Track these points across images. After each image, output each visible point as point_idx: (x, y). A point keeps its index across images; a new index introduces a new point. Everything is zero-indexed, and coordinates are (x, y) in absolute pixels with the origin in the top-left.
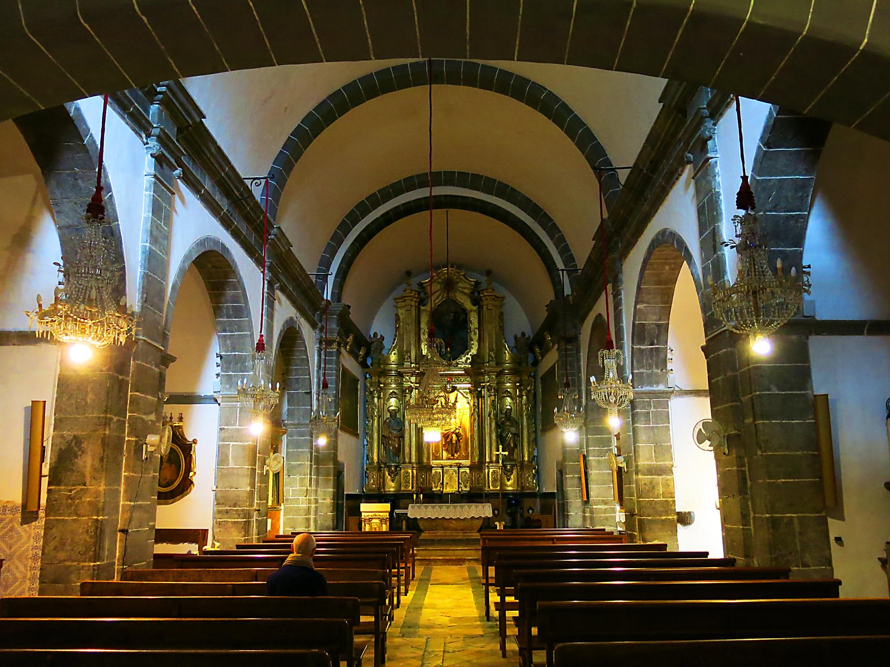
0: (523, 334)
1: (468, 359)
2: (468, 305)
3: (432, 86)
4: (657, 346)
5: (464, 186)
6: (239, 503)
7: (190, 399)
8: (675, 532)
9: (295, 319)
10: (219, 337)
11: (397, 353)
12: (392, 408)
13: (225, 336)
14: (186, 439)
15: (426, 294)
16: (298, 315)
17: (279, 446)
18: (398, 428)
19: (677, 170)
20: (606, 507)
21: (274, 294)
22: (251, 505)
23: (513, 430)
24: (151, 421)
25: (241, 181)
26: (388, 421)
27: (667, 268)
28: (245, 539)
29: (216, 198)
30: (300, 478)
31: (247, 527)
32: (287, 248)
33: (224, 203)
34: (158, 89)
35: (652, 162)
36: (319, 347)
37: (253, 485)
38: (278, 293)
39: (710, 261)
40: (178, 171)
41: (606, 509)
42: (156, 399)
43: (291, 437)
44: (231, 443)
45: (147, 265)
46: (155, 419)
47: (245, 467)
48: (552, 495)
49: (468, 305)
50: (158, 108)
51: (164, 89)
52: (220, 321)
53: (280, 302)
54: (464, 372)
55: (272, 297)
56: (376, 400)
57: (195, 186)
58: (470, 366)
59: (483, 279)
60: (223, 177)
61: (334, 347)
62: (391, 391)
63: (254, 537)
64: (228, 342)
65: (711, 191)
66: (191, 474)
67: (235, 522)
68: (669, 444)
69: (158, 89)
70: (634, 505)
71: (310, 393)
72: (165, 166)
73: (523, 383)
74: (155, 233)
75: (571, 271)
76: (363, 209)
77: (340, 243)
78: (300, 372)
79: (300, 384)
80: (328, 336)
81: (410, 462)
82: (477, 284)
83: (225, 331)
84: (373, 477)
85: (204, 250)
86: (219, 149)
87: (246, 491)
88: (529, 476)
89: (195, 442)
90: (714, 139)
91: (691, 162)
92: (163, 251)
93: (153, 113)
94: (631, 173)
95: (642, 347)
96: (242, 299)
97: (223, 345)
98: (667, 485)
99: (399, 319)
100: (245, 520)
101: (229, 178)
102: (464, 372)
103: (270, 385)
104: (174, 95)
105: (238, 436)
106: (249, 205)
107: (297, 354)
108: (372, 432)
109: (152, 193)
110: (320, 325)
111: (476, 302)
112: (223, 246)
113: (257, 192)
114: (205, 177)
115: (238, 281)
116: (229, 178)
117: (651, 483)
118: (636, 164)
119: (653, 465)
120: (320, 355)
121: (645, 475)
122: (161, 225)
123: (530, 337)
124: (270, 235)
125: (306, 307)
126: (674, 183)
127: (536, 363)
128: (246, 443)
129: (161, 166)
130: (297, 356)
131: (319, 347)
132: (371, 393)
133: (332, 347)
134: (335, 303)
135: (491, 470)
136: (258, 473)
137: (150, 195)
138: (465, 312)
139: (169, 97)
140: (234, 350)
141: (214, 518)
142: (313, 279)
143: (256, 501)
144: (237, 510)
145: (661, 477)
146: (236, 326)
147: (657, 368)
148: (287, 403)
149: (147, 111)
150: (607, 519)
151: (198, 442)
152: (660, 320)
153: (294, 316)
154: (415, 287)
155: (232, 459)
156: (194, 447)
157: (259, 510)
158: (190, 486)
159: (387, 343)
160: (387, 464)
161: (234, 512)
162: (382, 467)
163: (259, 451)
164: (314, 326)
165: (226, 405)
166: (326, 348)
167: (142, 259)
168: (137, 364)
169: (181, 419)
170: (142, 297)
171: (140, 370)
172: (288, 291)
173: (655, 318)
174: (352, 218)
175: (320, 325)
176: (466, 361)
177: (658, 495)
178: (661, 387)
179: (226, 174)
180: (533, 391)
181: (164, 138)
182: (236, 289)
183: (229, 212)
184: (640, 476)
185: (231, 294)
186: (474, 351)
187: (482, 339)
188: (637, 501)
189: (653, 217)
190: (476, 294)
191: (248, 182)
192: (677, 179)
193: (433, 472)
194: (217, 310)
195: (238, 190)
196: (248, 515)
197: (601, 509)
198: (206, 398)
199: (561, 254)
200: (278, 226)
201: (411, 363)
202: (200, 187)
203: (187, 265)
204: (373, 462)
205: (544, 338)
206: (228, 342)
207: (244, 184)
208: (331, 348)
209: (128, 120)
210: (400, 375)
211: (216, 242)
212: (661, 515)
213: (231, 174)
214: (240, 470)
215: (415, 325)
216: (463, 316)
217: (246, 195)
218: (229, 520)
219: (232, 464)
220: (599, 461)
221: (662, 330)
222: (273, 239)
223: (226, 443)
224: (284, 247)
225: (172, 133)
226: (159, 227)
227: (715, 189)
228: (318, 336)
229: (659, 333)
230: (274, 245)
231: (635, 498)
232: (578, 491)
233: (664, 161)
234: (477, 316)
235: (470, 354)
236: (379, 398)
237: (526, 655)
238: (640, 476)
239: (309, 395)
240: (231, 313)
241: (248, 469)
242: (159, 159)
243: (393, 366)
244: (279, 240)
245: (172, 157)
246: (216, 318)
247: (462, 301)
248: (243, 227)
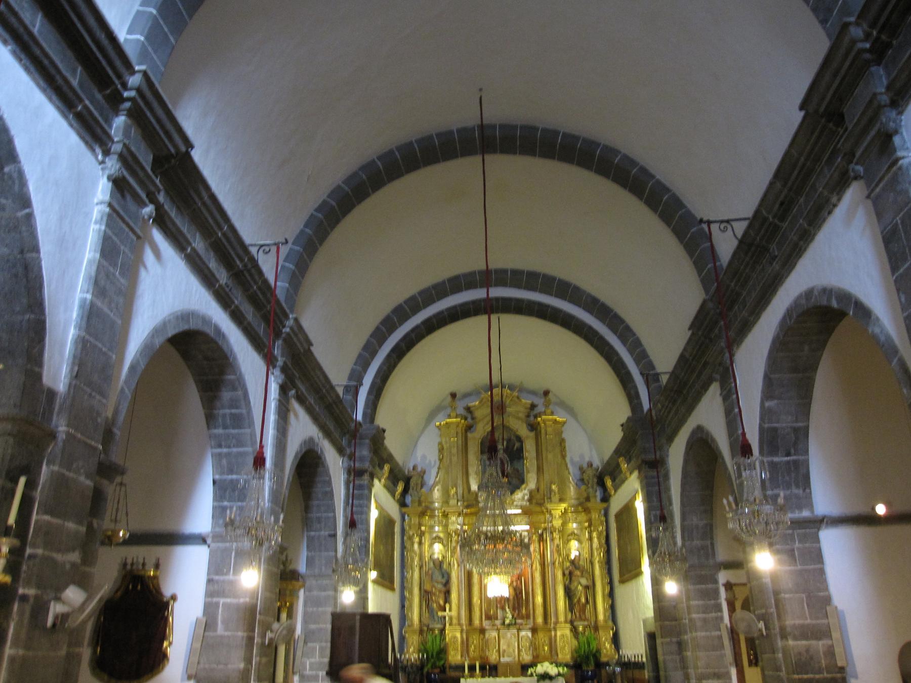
0: (590, 465)
1: (524, 495)
2: (523, 431)
3: (486, 157)
7: (174, 539)
16: (321, 435)
19: (828, 201)
23: (584, 581)
25: (244, 247)
32: (307, 347)
33: (223, 276)
34: (126, 94)
35: (782, 204)
37: (248, 660)
38: (295, 405)
40: (149, 209)
48: (639, 666)
49: (523, 431)
50: (125, 122)
51: (133, 94)
53: (296, 415)
57: (178, 241)
59: (540, 401)
60: (220, 239)
66: (165, 644)
69: (126, 94)
72: (128, 197)
74: (102, 283)
76: (401, 313)
77: (373, 354)
78: (323, 509)
79: (323, 524)
83: (220, 446)
86: (213, 198)
89: (174, 598)
90: (902, 134)
91: (862, 178)
93: (116, 128)
94: (750, 227)
96: (243, 403)
98: (830, 652)
103: (272, 518)
104: (147, 103)
105: (229, 589)
106: (256, 283)
110: (348, 451)
111: (533, 427)
112: (218, 330)
113: (268, 266)
120: (347, 488)
125: (332, 428)
126: (824, 220)
129: (123, 196)
138: (519, 439)
140: (231, 472)
142: (340, 391)
148: (306, 549)
149: (109, 122)
152: (797, 421)
159: (431, 478)
164: (341, 451)
167: (78, 315)
169: (157, 566)
170: (72, 370)
171: (60, 483)
174: (388, 325)
175: (348, 451)
176: (523, 498)
178: (806, 514)
181: (130, 159)
182: (234, 389)
184: (791, 642)
189: (786, 277)
190: (532, 418)
191: (253, 250)
192: (830, 213)
194: (210, 418)
195: (242, 260)
199: (637, 361)
202: (185, 244)
203: (159, 341)
206: (224, 461)
209: (73, 122)
210: (446, 515)
211: (206, 320)
213: (230, 235)
215: (462, 458)
216: (517, 445)
219: (220, 630)
221: (801, 436)
225: (146, 159)
226: (111, 277)
228: (346, 464)
229: (797, 438)
230: (289, 343)
233: (802, 200)
242: (118, 184)
244: (296, 335)
245: (142, 189)
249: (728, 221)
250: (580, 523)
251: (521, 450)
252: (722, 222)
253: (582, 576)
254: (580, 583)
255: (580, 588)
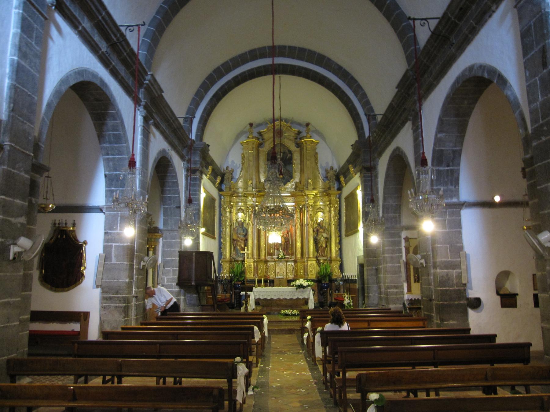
0: (332, 168)
2: (292, 147)
4: (452, 168)
5: (293, 57)
9: (167, 151)
10: (104, 160)
11: (242, 181)
12: (240, 220)
13: (108, 159)
14: (77, 241)
15: (263, 139)
16: (170, 148)
18: (243, 234)
19: (490, 7)
20: (397, 290)
21: (149, 128)
22: (130, 293)
23: (325, 235)
24: (20, 223)
26: (236, 229)
27: (466, 102)
28: (125, 320)
29: (95, 39)
31: (126, 310)
33: (104, 46)
36: (186, 174)
37: (131, 277)
38: (153, 129)
39: (537, 78)
41: (397, 292)
42: (26, 204)
43: (166, 239)
44: (114, 244)
45: (14, 77)
46: (25, 222)
49: (292, 147)
52: (104, 146)
54: (290, 195)
57: (73, 23)
58: (294, 190)
60: (100, 20)
61: (198, 174)
62: (239, 208)
63: (133, 317)
64: (111, 164)
65: (541, 11)
66: (82, 268)
67: (116, 307)
68: (461, 245)
71: (179, 207)
73: (332, 202)
74: (24, 49)
77: (202, 98)
79: (172, 201)
81: (253, 258)
83: (108, 154)
84: (226, 268)
85: (82, 79)
87: (126, 282)
88: (336, 267)
89: (85, 243)
92: (34, 68)
94: (439, 23)
95: (441, 168)
96: (120, 128)
97: (107, 167)
99: (244, 157)
100: (124, 305)
101: (106, 22)
102: (290, 195)
105: (119, 238)
106: (126, 51)
107: (170, 178)
108: (225, 236)
109: (21, 11)
111: (299, 145)
112: (102, 81)
114: (84, 18)
115: (116, 113)
116: (106, 22)
118: (445, 14)
119: (449, 261)
122: (31, 44)
123: (336, 169)
124: (145, 80)
127: (340, 189)
131: (186, 174)
132: (225, 209)
133: (196, 174)
134: (198, 142)
136: (136, 267)
137: (19, 13)
140: (115, 170)
141: (101, 303)
142: (181, 121)
144: (118, 297)
145: (455, 271)
146: (116, 151)
147: (452, 185)
150: (398, 299)
152: (455, 146)
153: (167, 149)
155: (114, 256)
156: (85, 247)
157: (136, 297)
158: (82, 277)
160: (236, 259)
161: (116, 299)
162: (232, 261)
163: (136, 250)
164: (182, 158)
165: (110, 214)
166: (190, 175)
167: (10, 71)
168: (3, 169)
169: (74, 225)
170: (9, 107)
172: (161, 128)
173: (451, 144)
176: (292, 187)
178: (455, 200)
179: (103, 18)
180: (338, 208)
182: (115, 119)
183: (107, 53)
185: (111, 124)
186: (297, 180)
190: (299, 140)
192: (490, 16)
193: (268, 264)
194: (101, 137)
195: (115, 36)
197: (394, 292)
198: (95, 208)
199: (363, 107)
200: (151, 73)
201: (253, 188)
202: (77, 24)
203: (64, 88)
206: (111, 164)
208: (196, 175)
210: (246, 196)
213: (107, 19)
216: (289, 155)
217: (121, 39)
219: (114, 261)
222: (147, 84)
223: (109, 244)
224: (157, 92)
227: (544, 9)
228: (186, 166)
230: (148, 90)
231: (432, 287)
232: (376, 279)
234: (299, 155)
235: (294, 182)
236: (230, 212)
237: (332, 393)
238: (438, 271)
239: (178, 209)
240: (112, 139)
241: (127, 264)
243: (240, 190)
246: (100, 143)
247: (289, 145)
248: (121, 69)
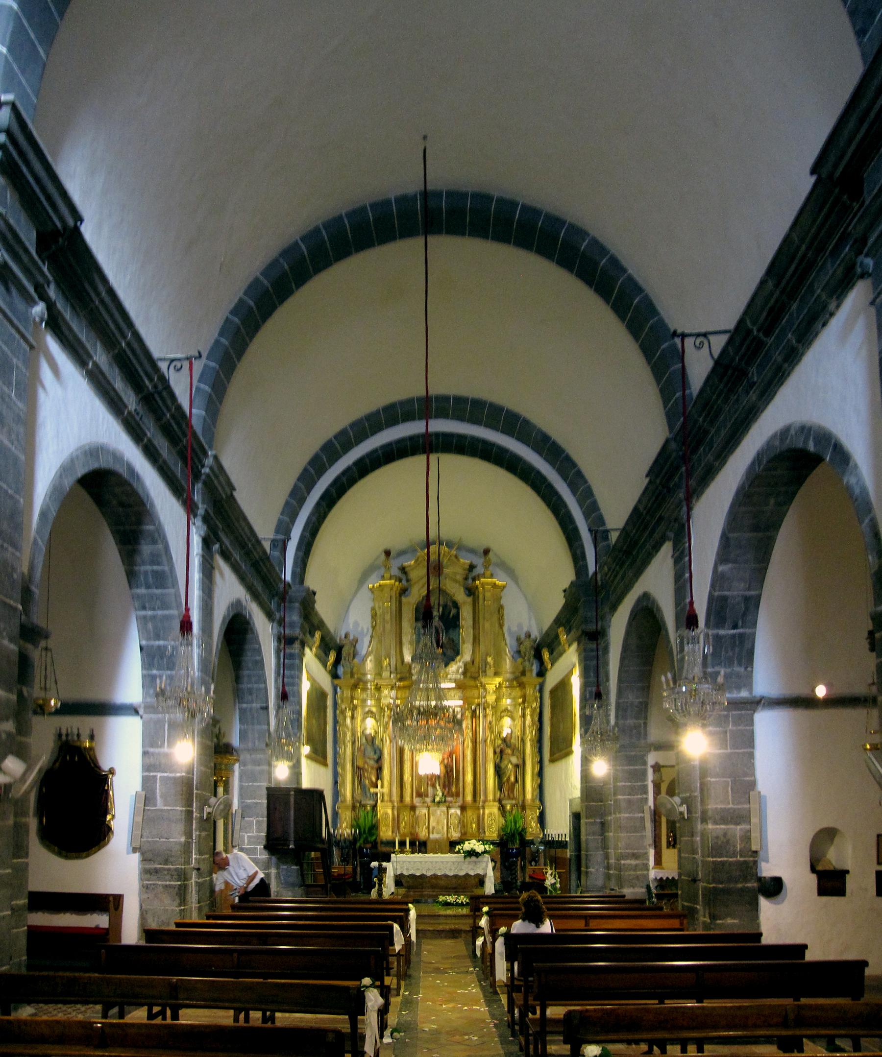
0: (528, 635)
2: (460, 596)
6: (171, 859)
8: (755, 907)
14: (99, 768)
16: (248, 597)
17: (231, 779)
19: (825, 306)
20: (637, 862)
22: (188, 862)
23: (514, 760)
30: (257, 821)
31: (182, 892)
32: (229, 493)
33: (131, 401)
37: (189, 834)
38: (220, 562)
40: (39, 309)
41: (636, 865)
44: (159, 775)
47: (178, 808)
48: (562, 845)
49: (460, 596)
53: (222, 574)
55: (209, 563)
56: (348, 721)
59: (479, 561)
66: (109, 817)
67: (166, 886)
70: (697, 867)
72: (14, 291)
75: (599, 534)
77: (301, 501)
78: (253, 679)
79: (254, 696)
80: (287, 631)
81: (391, 801)
82: (472, 567)
86: (111, 292)
87: (180, 843)
89: (112, 771)
91: (870, 275)
94: (730, 342)
96: (164, 558)
100: (179, 883)
106: (169, 410)
110: (277, 615)
111: (471, 592)
117: (725, 835)
119: (729, 809)
121: (717, 824)
127: (542, 673)
128: (178, 775)
130: (248, 658)
135: (487, 812)
138: (456, 605)
139: (13, 159)
141: (141, 879)
143: (194, 856)
144: (169, 870)
145: (739, 827)
147: (740, 664)
150: (637, 877)
151: (117, 771)
152: (749, 589)
154: (395, 571)
156: (112, 779)
157: (198, 869)
158: (108, 833)
159: (364, 647)
161: (166, 872)
163: (196, 785)
164: (270, 615)
169: (92, 737)
176: (458, 671)
177: (734, 853)
187: (477, 640)
188: (702, 861)
189: (762, 411)
190: (470, 581)
191: (163, 366)
195: (151, 380)
196: (183, 876)
197: (631, 864)
199: (587, 515)
202: (85, 357)
203: (69, 482)
204: (684, 817)
205: (557, 636)
206: (150, 626)
207: (157, 369)
211: (117, 457)
212: (736, 882)
213: (136, 345)
214: (171, 812)
215: (396, 623)
216: (453, 611)
218: (160, 883)
219: (160, 804)
220: (629, 801)
221: (752, 604)
228: (276, 631)
229: (747, 609)
231: (698, 857)
233: (794, 307)
238: (710, 826)
239: (265, 711)
241: (181, 811)
244: (217, 477)
248: (162, 445)
249: (705, 335)
250: (514, 699)
251: (457, 617)
252: (698, 335)
253: (513, 754)
254: (510, 762)
255: (510, 766)
